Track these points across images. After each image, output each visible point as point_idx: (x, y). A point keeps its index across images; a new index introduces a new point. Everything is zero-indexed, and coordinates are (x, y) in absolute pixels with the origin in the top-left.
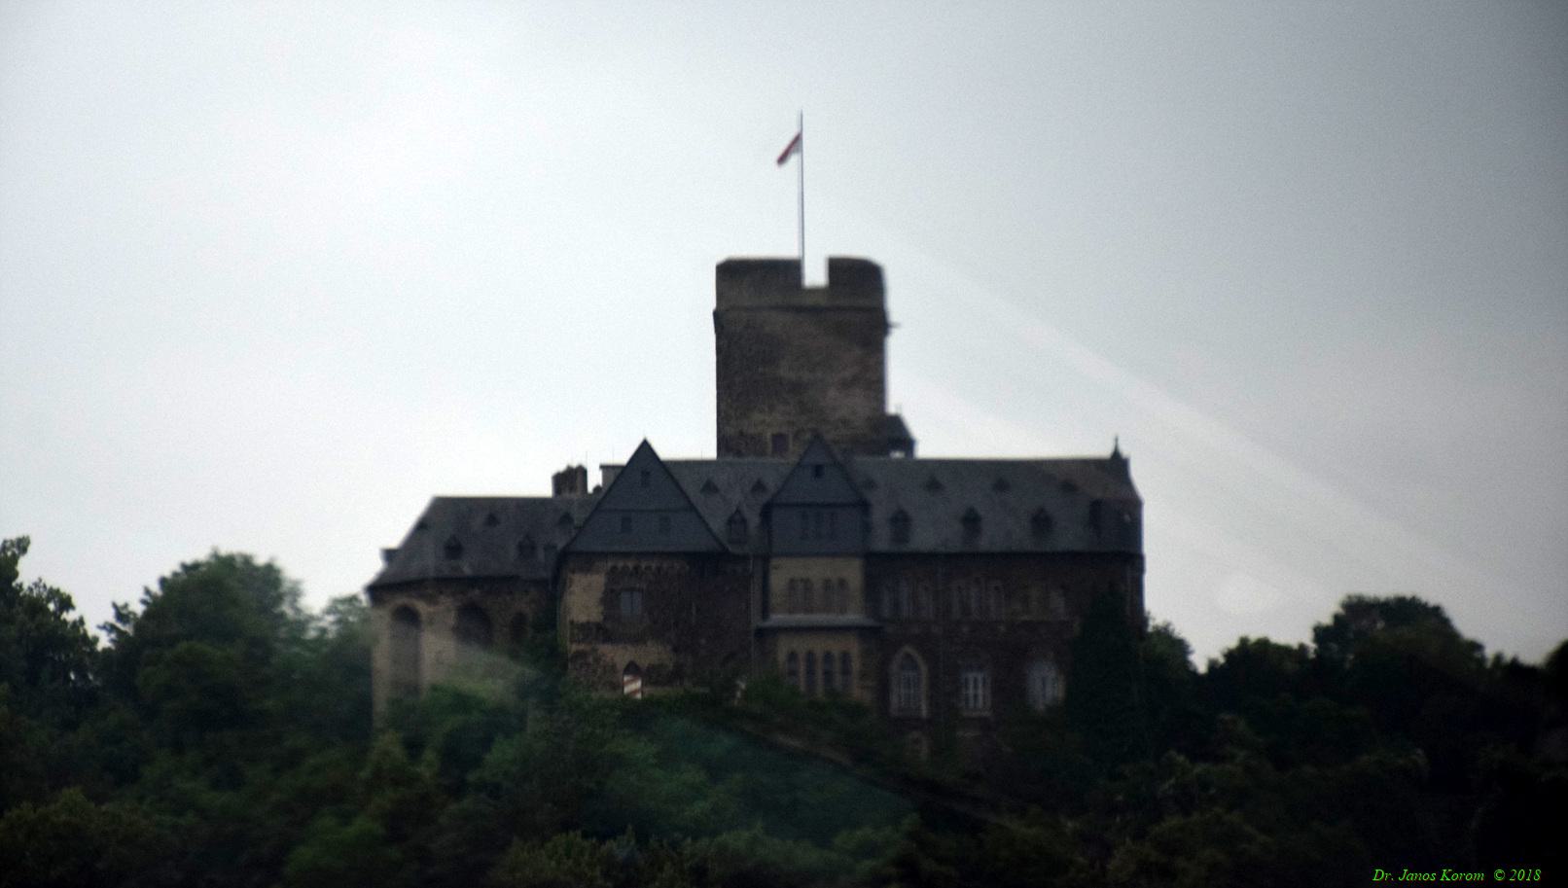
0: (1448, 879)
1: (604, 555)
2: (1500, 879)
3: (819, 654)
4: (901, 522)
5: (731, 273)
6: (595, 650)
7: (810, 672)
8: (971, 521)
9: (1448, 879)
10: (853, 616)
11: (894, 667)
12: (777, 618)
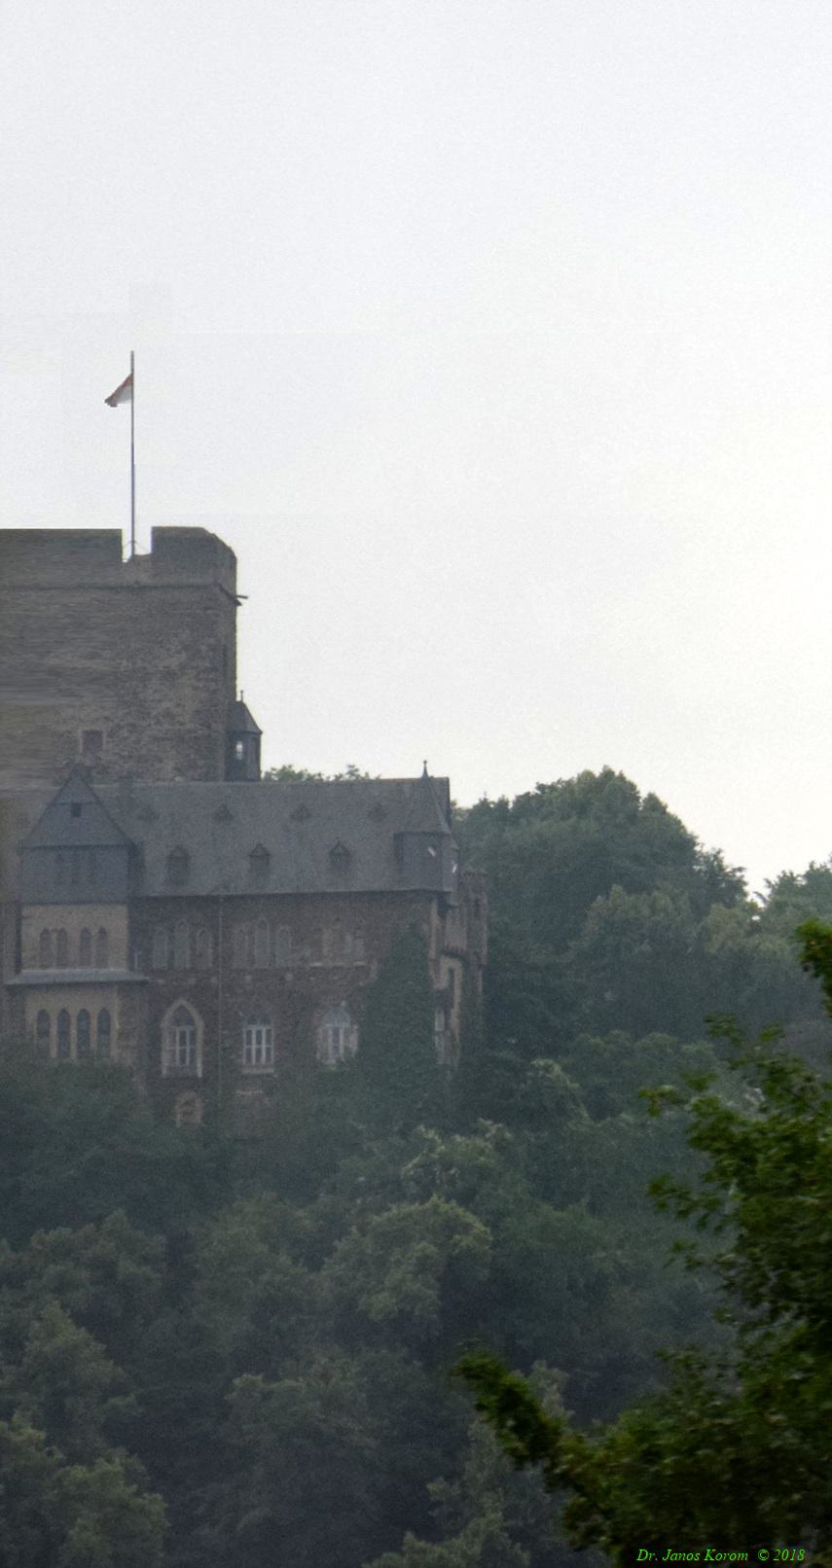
0: (712, 1559)
2: (764, 1559)
3: (74, 1012)
4: (180, 860)
7: (64, 1033)
9: (712, 1559)
10: (117, 969)
11: (166, 1023)
12: (31, 973)
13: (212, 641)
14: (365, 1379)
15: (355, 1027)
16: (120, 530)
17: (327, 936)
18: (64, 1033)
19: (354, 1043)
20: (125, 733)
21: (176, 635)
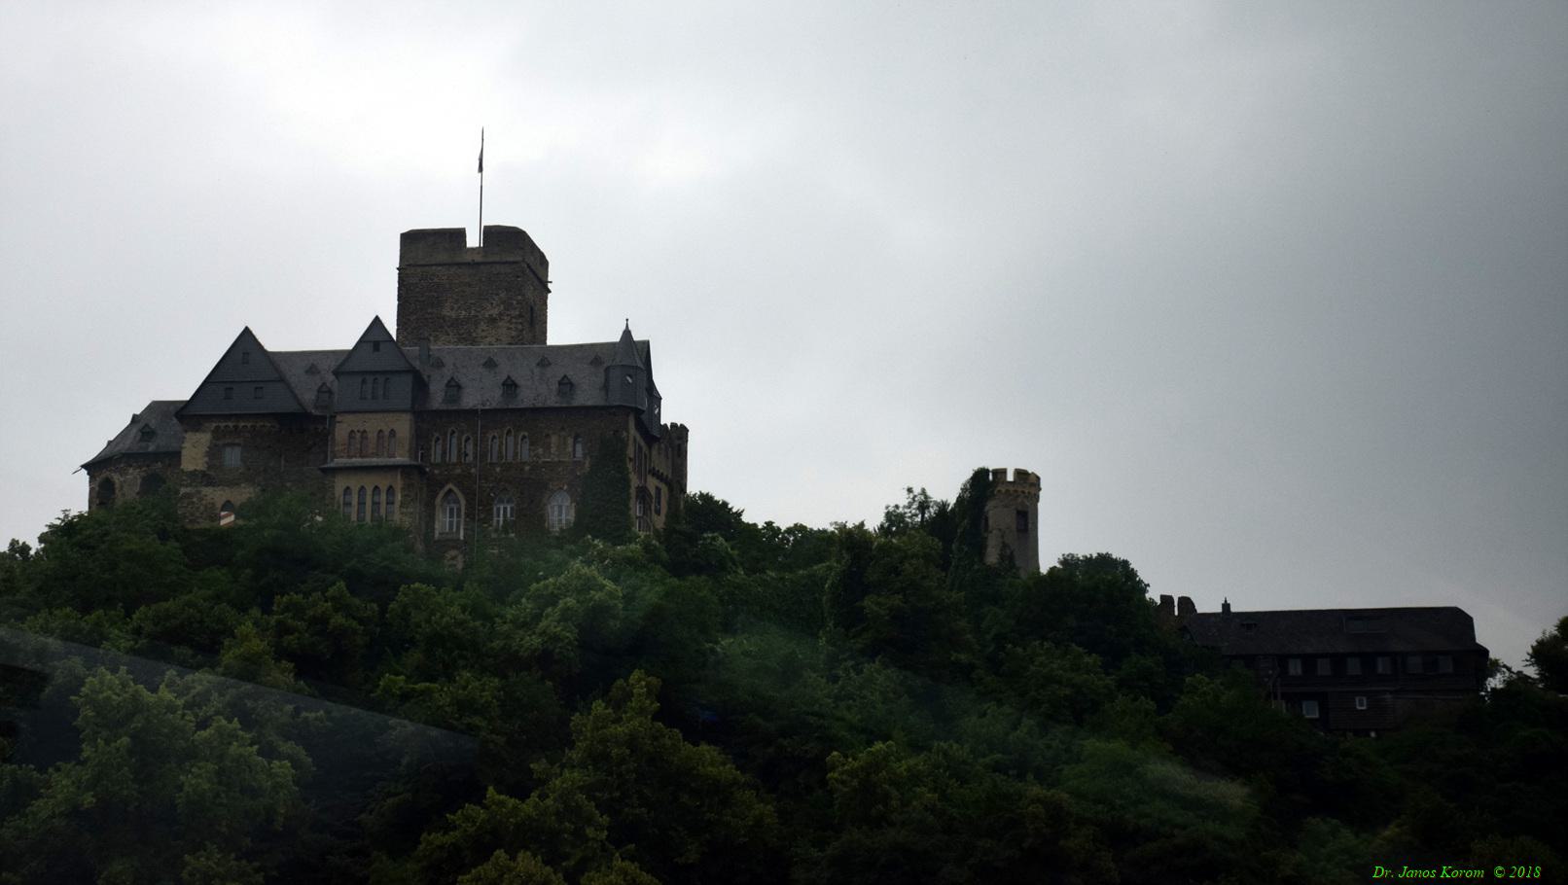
0: (1448, 876)
1: (209, 418)
2: (1500, 876)
4: (454, 387)
6: (199, 492)
7: (362, 503)
8: (510, 386)
9: (1448, 876)
10: (401, 459)
13: (520, 297)
15: (573, 505)
17: (554, 439)
18: (362, 503)
19: (572, 517)
21: (497, 294)
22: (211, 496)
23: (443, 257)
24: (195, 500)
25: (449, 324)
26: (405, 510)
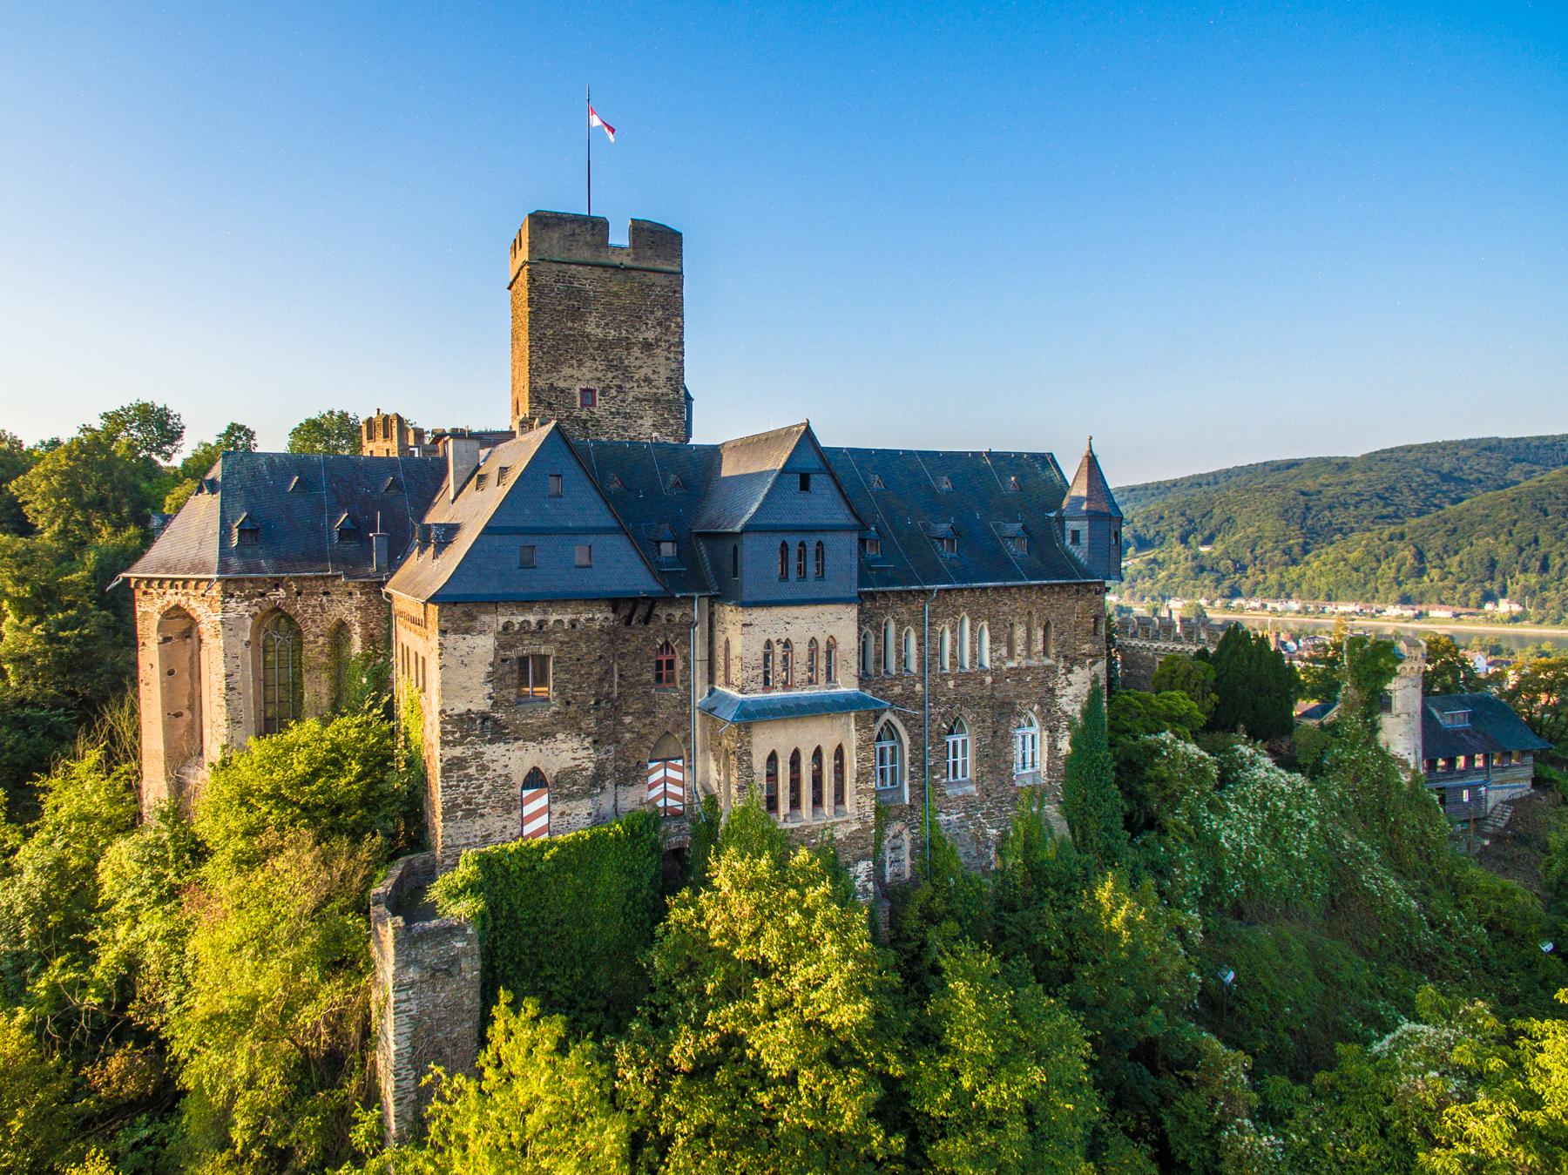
5: (541, 222)
6: (478, 755)
14: (726, 941)
16: (530, 216)
20: (613, 392)
22: (503, 761)
23: (585, 254)
24: (472, 771)
25: (596, 345)
26: (863, 786)
